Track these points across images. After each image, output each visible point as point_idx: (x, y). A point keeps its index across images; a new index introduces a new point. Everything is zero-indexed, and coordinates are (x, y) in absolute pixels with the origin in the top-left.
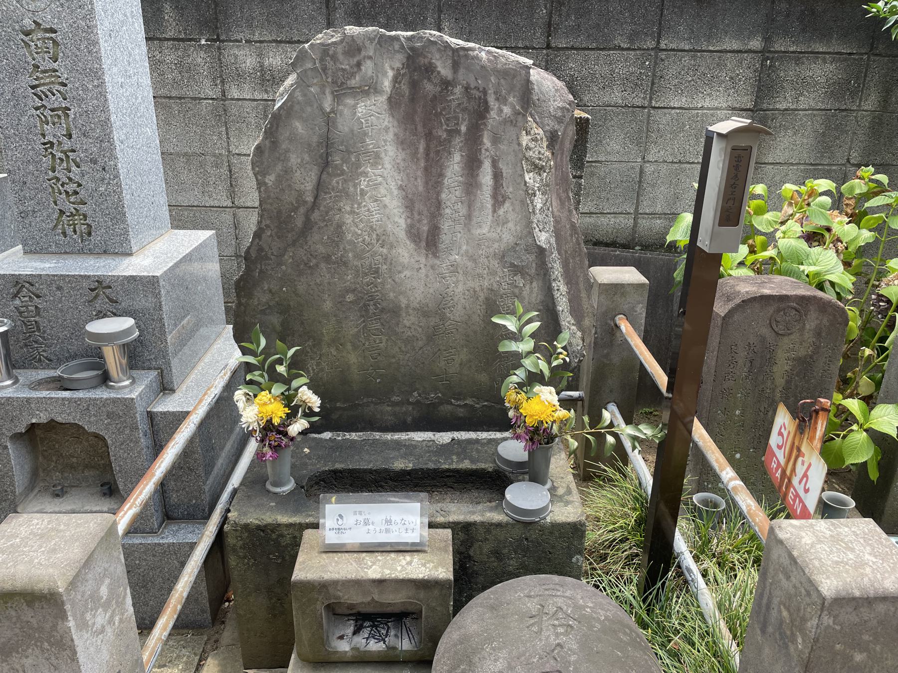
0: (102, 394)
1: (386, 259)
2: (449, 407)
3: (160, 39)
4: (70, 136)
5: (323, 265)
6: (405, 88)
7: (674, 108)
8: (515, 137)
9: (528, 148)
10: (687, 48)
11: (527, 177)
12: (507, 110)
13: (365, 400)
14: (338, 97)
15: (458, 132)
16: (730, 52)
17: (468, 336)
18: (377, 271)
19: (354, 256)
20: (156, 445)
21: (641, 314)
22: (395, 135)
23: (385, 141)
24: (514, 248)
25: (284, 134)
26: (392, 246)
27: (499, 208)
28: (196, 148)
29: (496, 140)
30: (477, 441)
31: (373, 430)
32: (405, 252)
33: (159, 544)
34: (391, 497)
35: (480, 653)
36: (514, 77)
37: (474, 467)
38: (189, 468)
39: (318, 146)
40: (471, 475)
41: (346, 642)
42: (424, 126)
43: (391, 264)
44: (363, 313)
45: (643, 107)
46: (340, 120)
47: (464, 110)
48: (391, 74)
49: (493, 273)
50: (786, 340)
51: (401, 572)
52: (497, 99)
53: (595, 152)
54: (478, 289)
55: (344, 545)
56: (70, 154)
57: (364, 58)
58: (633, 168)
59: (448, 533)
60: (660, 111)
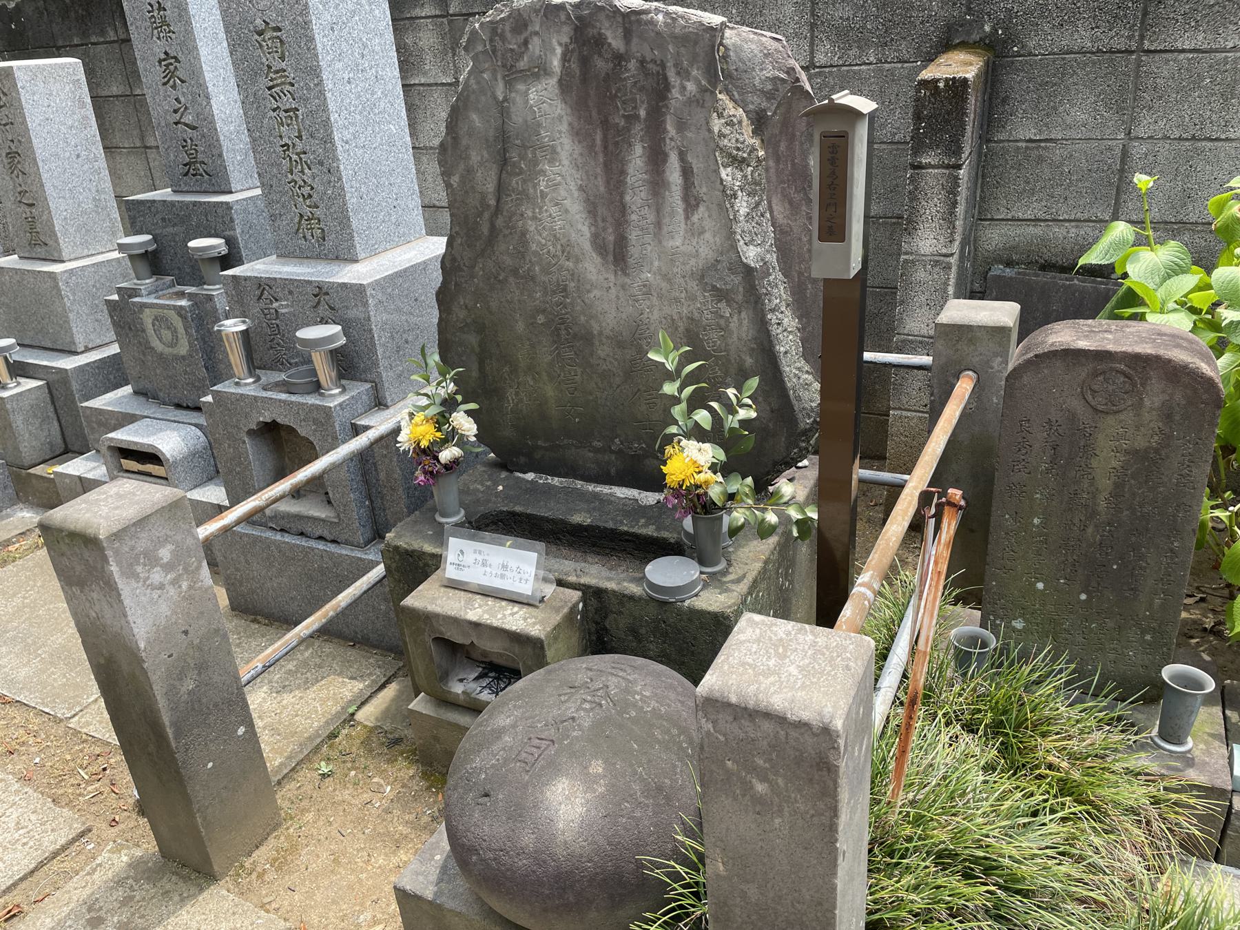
0: (311, 400)
4: (300, 137)
5: (511, 279)
6: (575, 66)
7: (1183, 51)
9: (722, 135)
11: (724, 173)
12: (691, 86)
14: (509, 84)
15: (637, 117)
18: (565, 290)
25: (463, 129)
29: (681, 126)
32: (593, 267)
34: (510, 541)
36: (696, 43)
42: (599, 113)
46: (513, 109)
47: (642, 89)
48: (559, 51)
49: (692, 298)
50: (1110, 420)
52: (678, 73)
53: (1046, 125)
54: (675, 317)
55: (467, 583)
58: (1110, 149)
59: (577, 595)
60: (1157, 56)
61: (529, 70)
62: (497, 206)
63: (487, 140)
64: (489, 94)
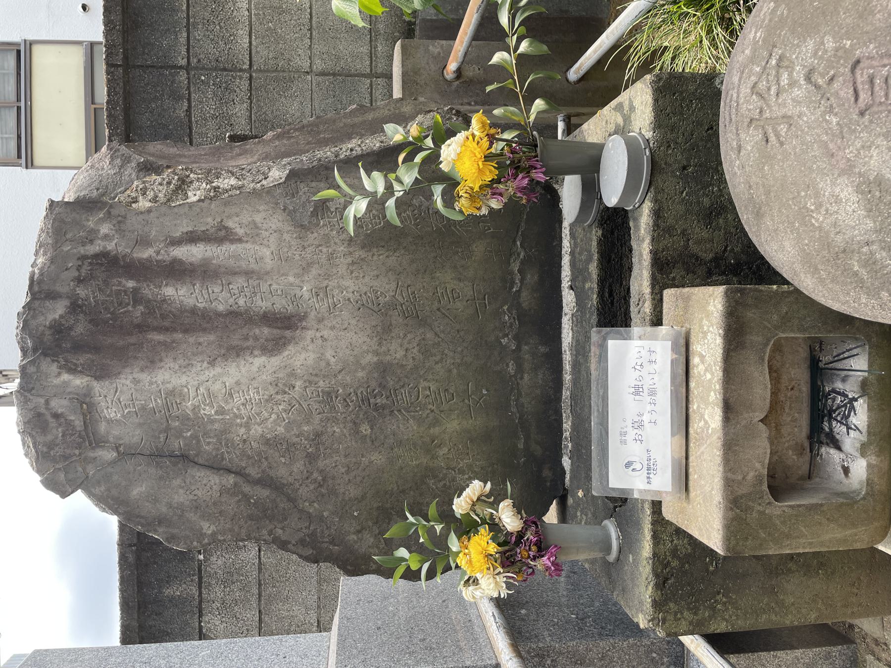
1: (310, 383)
2: (524, 294)
3: (200, 602)
5: (321, 464)
6: (82, 359)
7: (250, 43)
9: (155, 199)
10: (185, 35)
11: (193, 198)
12: (105, 229)
13: (514, 410)
14: (97, 442)
15: (135, 291)
17: (418, 271)
19: (308, 423)
21: (442, 46)
22: (142, 370)
23: (151, 383)
24: (291, 214)
26: (293, 374)
27: (236, 234)
29: (143, 241)
30: (572, 254)
31: (558, 399)
32: (300, 356)
35: (827, 233)
36: (62, 221)
37: (596, 257)
39: (161, 468)
40: (609, 261)
41: (852, 464)
42: (130, 334)
43: (316, 375)
44: (387, 412)
47: (106, 282)
48: (66, 377)
51: (712, 374)
52: (91, 242)
54: (349, 260)
57: (47, 409)
58: (318, 84)
59: (668, 294)
60: (254, 59)
62: (237, 473)
63: (161, 478)
64: (110, 469)
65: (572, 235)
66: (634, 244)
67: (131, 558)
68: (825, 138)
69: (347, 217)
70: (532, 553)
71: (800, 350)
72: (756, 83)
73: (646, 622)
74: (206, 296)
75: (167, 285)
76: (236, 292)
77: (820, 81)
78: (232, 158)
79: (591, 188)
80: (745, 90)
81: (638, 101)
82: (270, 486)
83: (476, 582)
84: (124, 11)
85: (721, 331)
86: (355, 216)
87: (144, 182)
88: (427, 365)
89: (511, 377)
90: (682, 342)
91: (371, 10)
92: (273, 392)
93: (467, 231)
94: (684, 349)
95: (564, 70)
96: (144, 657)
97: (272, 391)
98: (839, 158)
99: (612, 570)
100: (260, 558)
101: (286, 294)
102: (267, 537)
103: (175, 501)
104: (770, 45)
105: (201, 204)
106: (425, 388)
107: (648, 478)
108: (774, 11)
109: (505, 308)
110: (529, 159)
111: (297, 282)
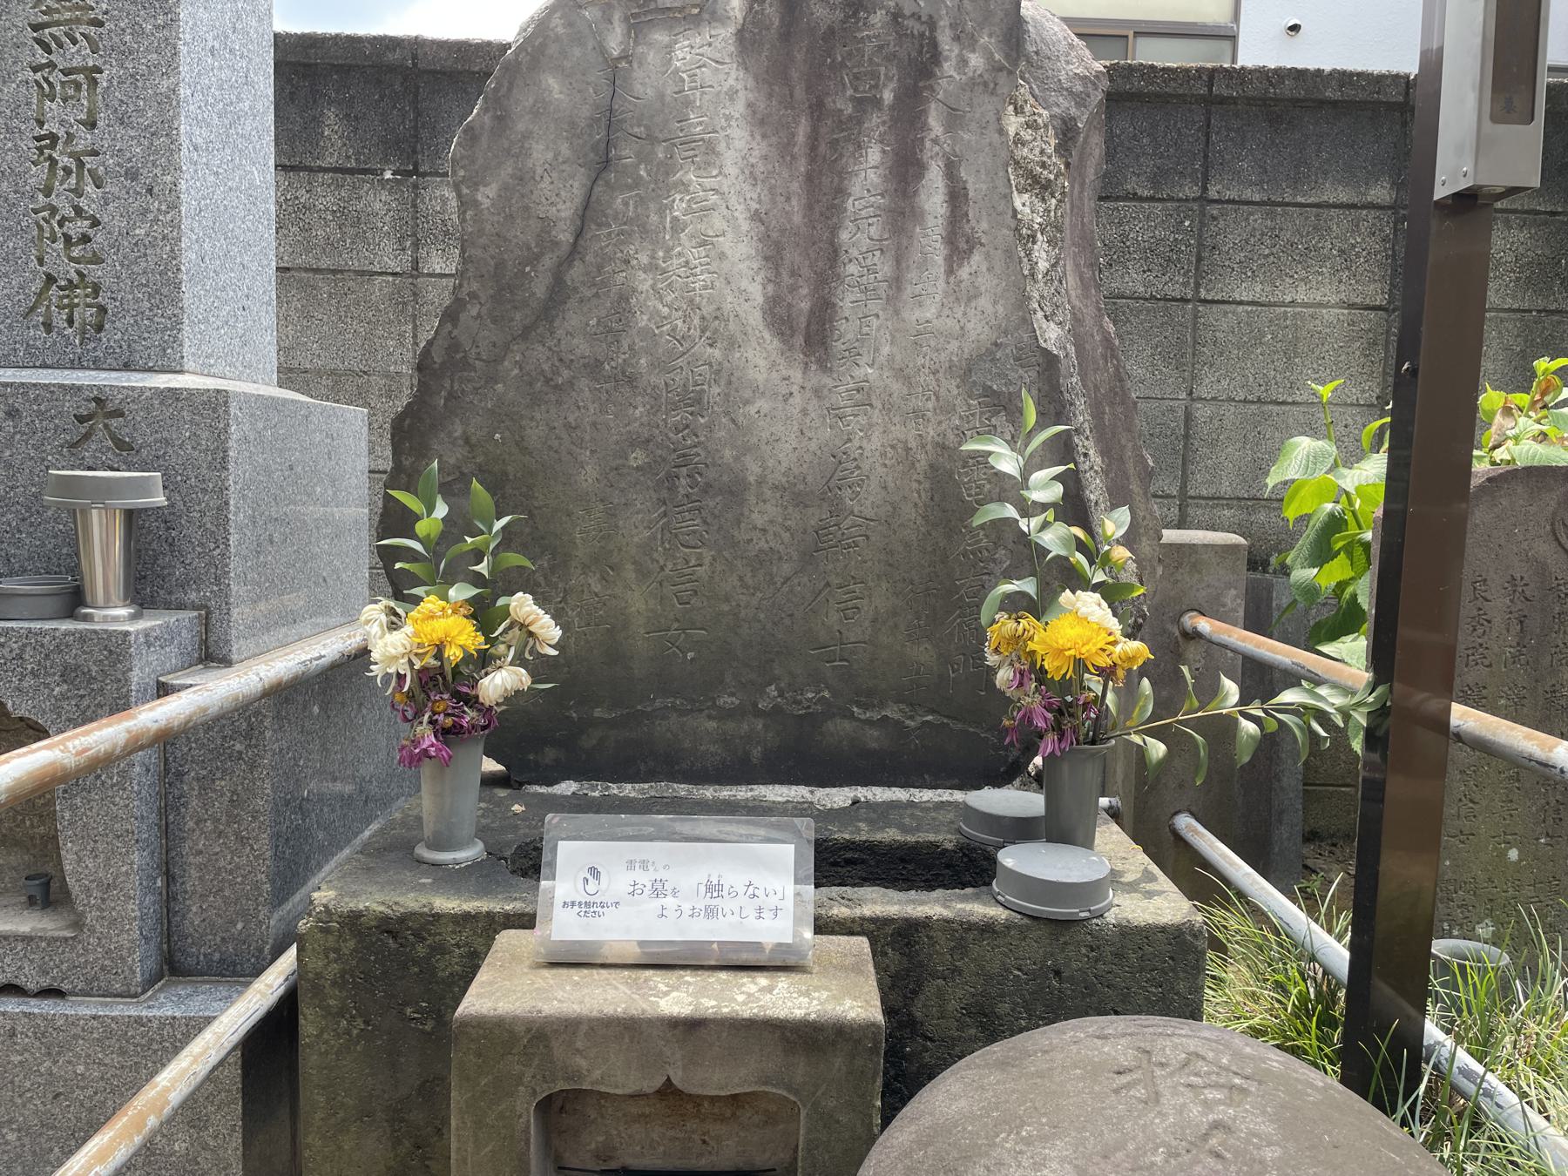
1: (718, 372)
2: (847, 726)
3: (310, 170)
4: (91, 124)
5: (583, 383)
7: (1241, 303)
8: (991, 117)
9: (1018, 141)
10: (1257, 198)
12: (976, 61)
13: (658, 703)
14: (636, 28)
15: (877, 103)
16: (1335, 206)
17: (891, 553)
20: (167, 771)
22: (749, 105)
26: (732, 344)
27: (960, 266)
28: (354, 361)
29: (954, 120)
30: (911, 804)
31: (673, 777)
32: (761, 359)
33: (139, 1021)
37: (911, 839)
38: (237, 834)
40: (902, 860)
42: (809, 89)
43: (730, 383)
44: (665, 494)
45: (1184, 300)
46: (638, 74)
51: (744, 1003)
52: (957, 38)
54: (913, 444)
56: (86, 159)
58: (1172, 410)
59: (862, 943)
60: (1215, 307)
61: (681, 9)
65: (941, 805)
66: (939, 893)
67: (393, 57)
68: (1131, 1147)
69: (992, 442)
70: (441, 717)
71: (768, 1155)
72: (1204, 1059)
73: (324, 901)
74: (864, 213)
75: (884, 152)
76: (869, 262)
77: (1213, 1142)
78: (1077, 265)
79: (1022, 830)
80: (1192, 1045)
81: (1167, 905)
82: (551, 298)
83: (393, 627)
84: (1295, 102)
85: (813, 1016)
86: (990, 453)
87: (1046, 126)
88: (738, 563)
89: (714, 700)
90: (791, 961)
91: (1292, 498)
92: (704, 312)
93: (951, 634)
94: (781, 964)
95: (1193, 809)
96: (256, 74)
97: (707, 310)
98: (1103, 1166)
99: (399, 852)
100: (381, 274)
101: (863, 341)
102: (465, 289)
103: (534, 146)
104: (1261, 1077)
105: (1010, 213)
106: (700, 557)
107: (573, 904)
108: (1312, 1086)
109: (826, 694)
110: (1075, 730)
111: (882, 359)
